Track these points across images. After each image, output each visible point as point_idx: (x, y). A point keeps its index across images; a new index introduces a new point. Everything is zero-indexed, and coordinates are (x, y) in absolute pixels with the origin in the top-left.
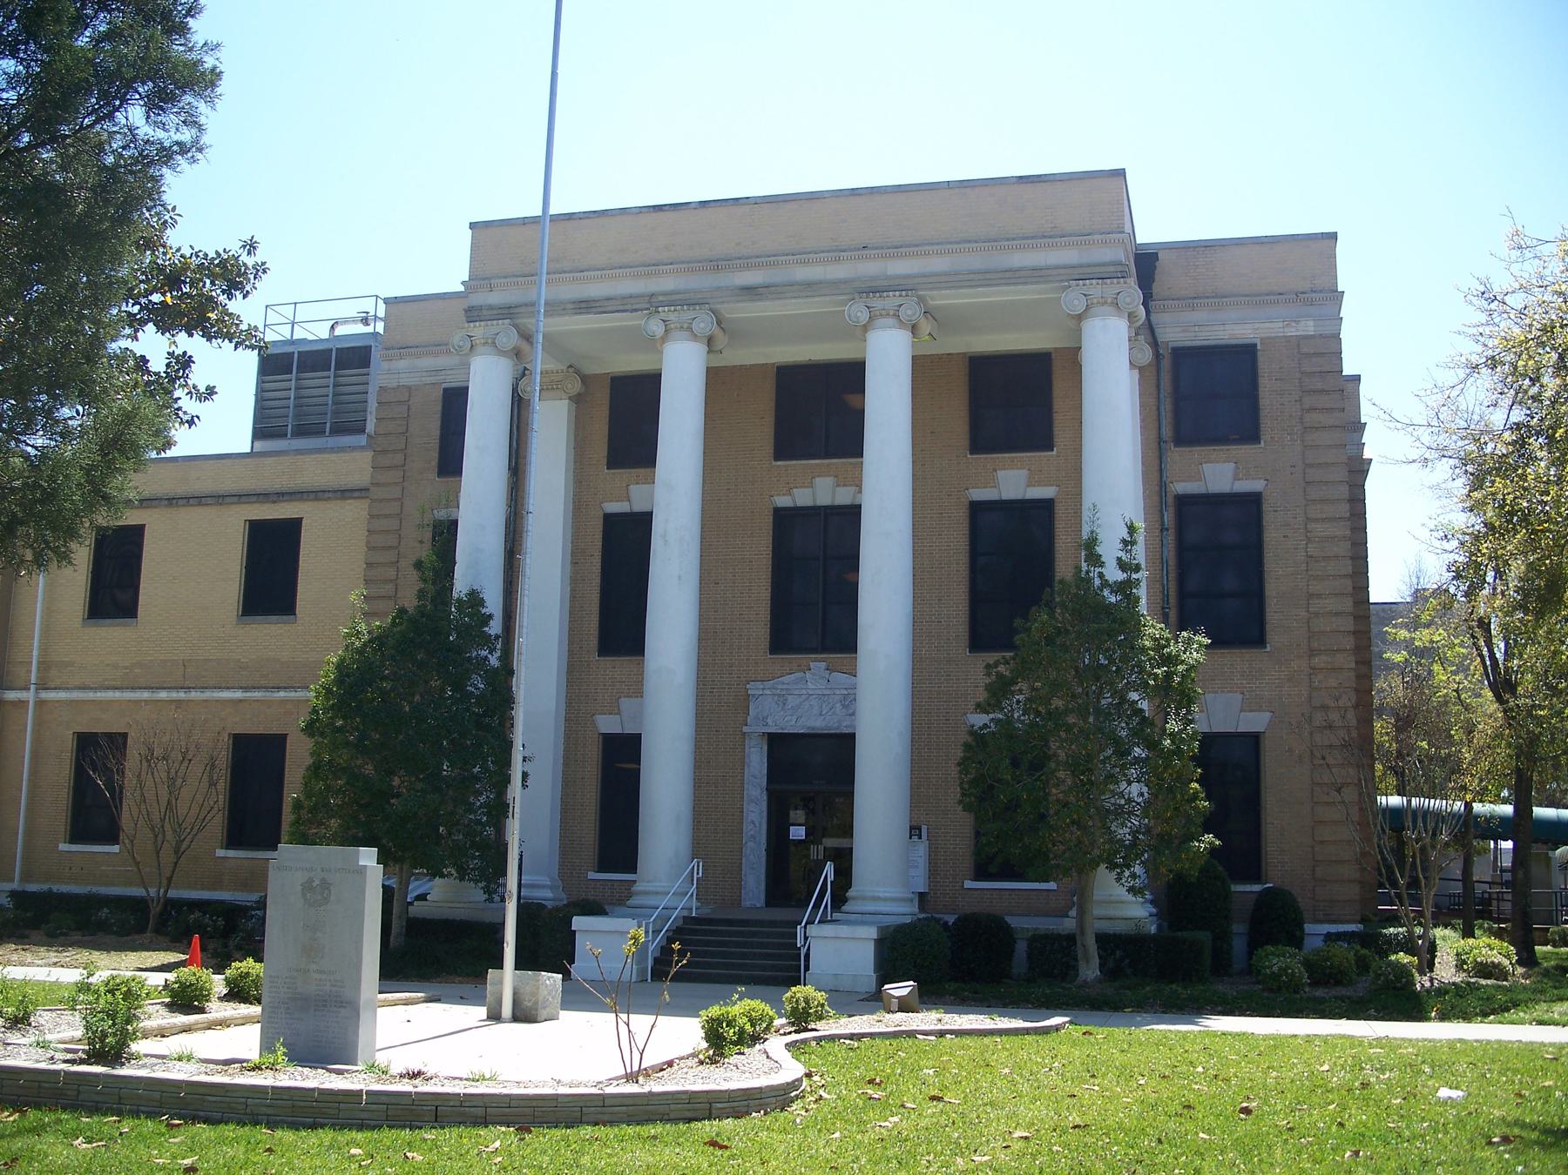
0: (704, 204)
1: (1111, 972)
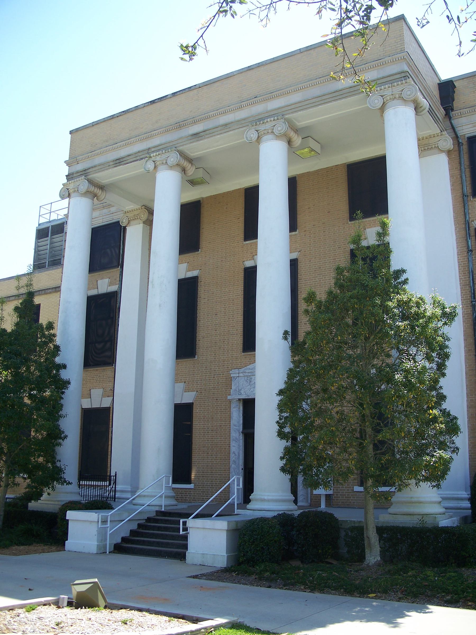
0: (174, 94)
1: (388, 555)
